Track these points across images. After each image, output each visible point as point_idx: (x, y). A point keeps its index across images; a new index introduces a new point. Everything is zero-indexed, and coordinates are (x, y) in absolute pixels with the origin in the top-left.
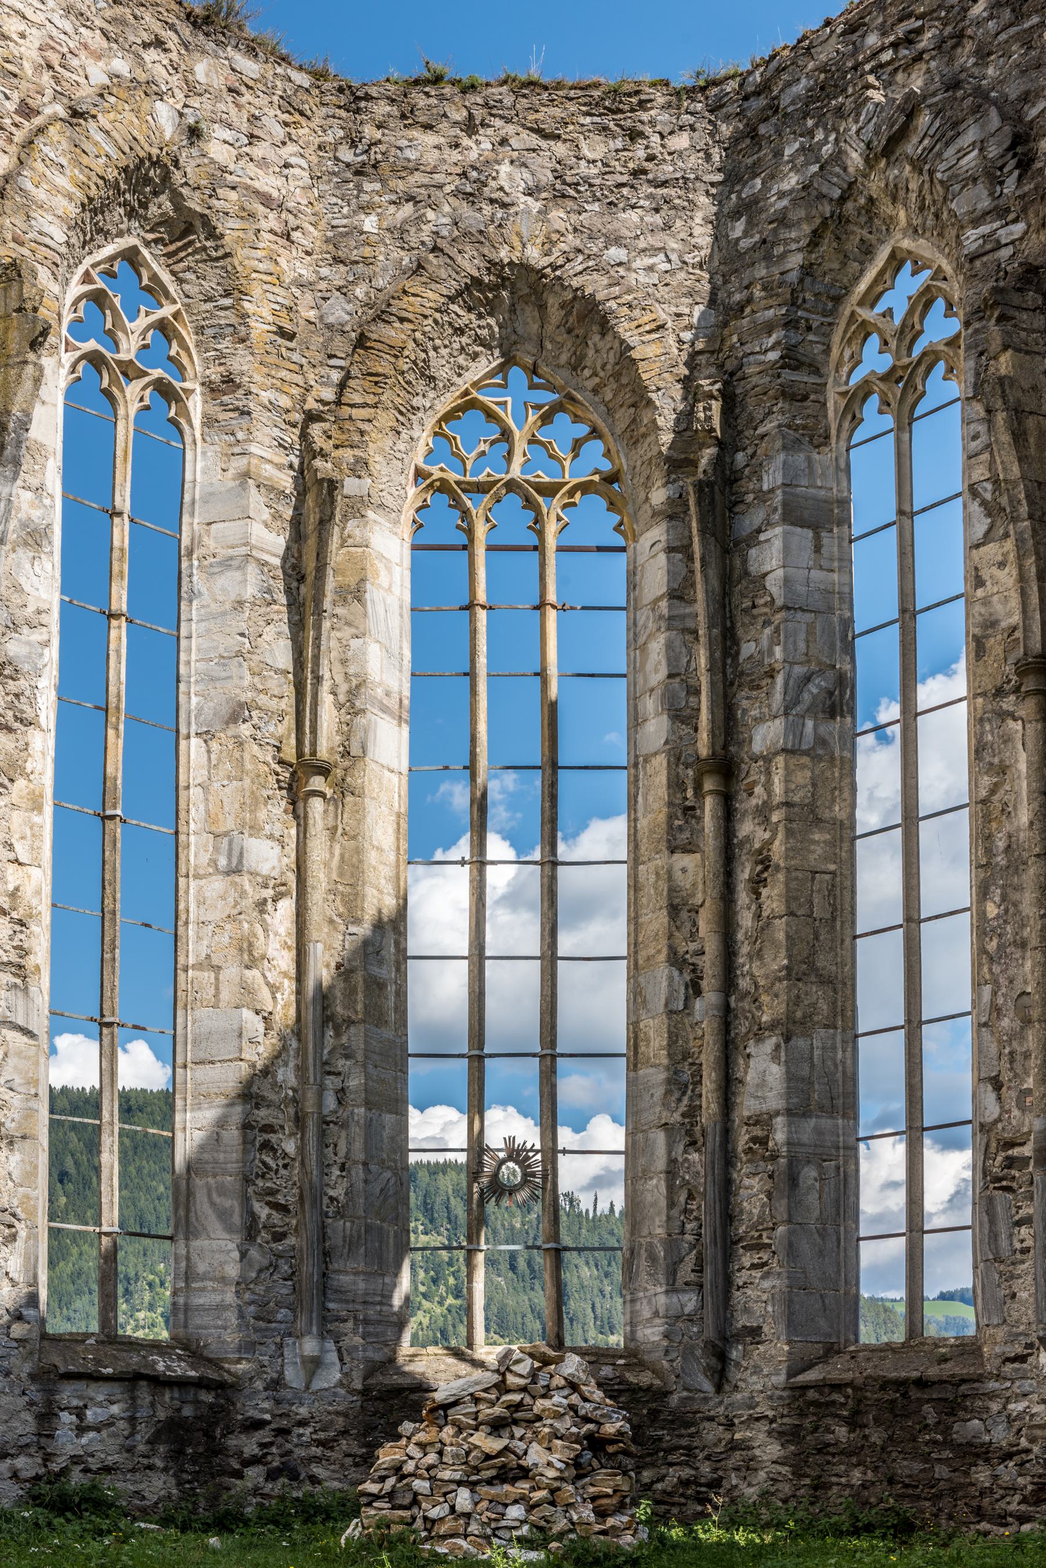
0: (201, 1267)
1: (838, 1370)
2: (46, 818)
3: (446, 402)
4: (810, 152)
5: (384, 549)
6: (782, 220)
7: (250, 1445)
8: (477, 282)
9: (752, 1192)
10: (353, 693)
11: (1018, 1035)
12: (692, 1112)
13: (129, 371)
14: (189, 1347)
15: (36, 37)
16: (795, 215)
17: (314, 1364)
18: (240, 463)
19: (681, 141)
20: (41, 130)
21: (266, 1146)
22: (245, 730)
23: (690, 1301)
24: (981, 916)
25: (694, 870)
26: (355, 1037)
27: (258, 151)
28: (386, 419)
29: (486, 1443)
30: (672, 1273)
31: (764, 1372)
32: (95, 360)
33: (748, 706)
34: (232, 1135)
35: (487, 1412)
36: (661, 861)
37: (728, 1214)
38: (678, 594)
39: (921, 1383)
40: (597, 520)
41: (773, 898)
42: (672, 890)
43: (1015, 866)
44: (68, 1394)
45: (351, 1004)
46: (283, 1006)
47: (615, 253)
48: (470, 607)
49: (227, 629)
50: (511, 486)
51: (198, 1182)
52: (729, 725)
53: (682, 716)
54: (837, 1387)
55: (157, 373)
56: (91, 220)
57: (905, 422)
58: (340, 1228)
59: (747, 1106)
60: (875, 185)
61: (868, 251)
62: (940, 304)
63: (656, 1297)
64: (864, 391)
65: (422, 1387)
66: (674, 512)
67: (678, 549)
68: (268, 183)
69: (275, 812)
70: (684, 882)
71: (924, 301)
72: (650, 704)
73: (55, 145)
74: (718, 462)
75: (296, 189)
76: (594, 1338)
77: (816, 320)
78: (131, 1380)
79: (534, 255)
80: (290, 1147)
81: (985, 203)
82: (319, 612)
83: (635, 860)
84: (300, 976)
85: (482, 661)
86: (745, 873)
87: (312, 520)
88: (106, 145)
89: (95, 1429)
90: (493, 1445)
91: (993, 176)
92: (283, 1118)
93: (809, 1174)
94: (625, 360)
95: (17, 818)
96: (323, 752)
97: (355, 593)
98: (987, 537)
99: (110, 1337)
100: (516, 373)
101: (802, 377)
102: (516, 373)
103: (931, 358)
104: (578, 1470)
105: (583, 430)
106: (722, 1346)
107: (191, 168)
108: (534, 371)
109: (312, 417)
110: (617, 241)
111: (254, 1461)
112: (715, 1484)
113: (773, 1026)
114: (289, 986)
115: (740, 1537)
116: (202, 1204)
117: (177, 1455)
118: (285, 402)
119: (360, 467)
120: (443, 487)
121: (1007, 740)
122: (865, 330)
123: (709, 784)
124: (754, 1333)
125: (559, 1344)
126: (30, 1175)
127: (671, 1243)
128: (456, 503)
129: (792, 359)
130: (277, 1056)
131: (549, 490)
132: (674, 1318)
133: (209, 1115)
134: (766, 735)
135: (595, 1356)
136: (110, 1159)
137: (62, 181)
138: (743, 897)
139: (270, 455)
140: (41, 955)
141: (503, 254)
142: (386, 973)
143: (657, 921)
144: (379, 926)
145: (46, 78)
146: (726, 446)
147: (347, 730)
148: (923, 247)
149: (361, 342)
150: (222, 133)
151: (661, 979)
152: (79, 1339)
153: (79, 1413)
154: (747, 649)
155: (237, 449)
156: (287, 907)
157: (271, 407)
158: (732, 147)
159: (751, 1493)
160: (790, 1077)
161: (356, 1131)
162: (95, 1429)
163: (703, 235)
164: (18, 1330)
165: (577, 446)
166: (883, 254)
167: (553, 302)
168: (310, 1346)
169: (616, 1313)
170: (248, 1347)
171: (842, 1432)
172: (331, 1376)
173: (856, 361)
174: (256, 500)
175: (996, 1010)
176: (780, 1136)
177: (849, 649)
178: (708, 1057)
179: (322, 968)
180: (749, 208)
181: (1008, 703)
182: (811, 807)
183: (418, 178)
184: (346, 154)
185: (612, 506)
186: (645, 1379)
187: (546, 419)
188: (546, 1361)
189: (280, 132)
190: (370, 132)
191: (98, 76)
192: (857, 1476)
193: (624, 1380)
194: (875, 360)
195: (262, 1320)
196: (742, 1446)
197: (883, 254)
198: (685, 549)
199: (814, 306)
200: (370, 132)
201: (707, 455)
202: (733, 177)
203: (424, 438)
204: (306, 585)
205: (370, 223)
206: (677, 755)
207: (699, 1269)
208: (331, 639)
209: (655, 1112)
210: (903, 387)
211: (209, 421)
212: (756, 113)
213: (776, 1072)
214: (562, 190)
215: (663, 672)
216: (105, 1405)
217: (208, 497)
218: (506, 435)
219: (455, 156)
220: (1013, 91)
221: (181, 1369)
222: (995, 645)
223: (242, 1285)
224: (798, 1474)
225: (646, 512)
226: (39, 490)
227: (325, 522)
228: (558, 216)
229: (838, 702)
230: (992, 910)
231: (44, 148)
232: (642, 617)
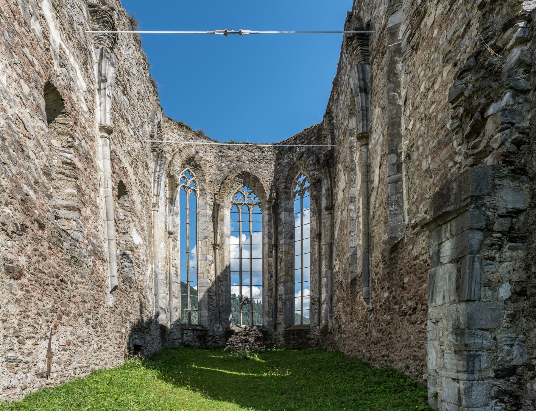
0: (202, 315)
1: (291, 328)
2: (179, 254)
3: (235, 191)
4: (289, 157)
5: (226, 213)
6: (285, 167)
7: (210, 339)
8: (240, 174)
9: (280, 304)
10: (222, 234)
11: (315, 284)
12: (271, 294)
13: (189, 188)
14: (202, 326)
15: (174, 139)
16: (287, 166)
17: (218, 328)
18: (205, 201)
19: (270, 153)
20: (175, 154)
21: (211, 298)
22: (207, 240)
23: (271, 319)
24: (311, 268)
25: (272, 260)
26: (223, 283)
27: (207, 154)
28: (226, 194)
29: (243, 337)
30: (269, 315)
31: (281, 329)
32: (184, 186)
33: (279, 237)
34: (206, 296)
35: (243, 334)
36: (267, 259)
38: (269, 221)
39: (302, 330)
40: (257, 209)
41: (283, 264)
42: (269, 263)
43: (315, 262)
44: (185, 332)
45: (223, 278)
46: (213, 279)
47: (260, 170)
48: (239, 222)
49: (204, 225)
50: (245, 204)
51: (202, 303)
52: (277, 240)
53: (270, 238)
54: (291, 331)
55: (193, 188)
56: (183, 166)
57: (302, 198)
58: (222, 309)
59: (279, 293)
60: (298, 163)
61: (297, 172)
62: (307, 181)
63: (266, 319)
64: (296, 192)
65: (233, 331)
66: (269, 209)
67: (269, 214)
69: (212, 251)
70: (270, 262)
71: (304, 181)
72: (265, 236)
73: (177, 156)
74: (275, 202)
75: (212, 159)
76: (257, 324)
77: (289, 182)
78: (193, 330)
79: (248, 170)
80: (214, 298)
81: (313, 169)
82: (217, 223)
83: (263, 258)
84: (215, 275)
85: (241, 229)
86: (279, 261)
87: (216, 210)
88: (185, 156)
89: (189, 336)
90: (245, 338)
91: (314, 165)
92: (213, 294)
93: (288, 302)
94: (262, 186)
95: (176, 253)
96: (218, 243)
97: (222, 220)
98: (312, 216)
99: (190, 324)
100: (246, 187)
101: (288, 190)
102: (246, 187)
103: (305, 189)
104: (256, 341)
105: (255, 196)
106: (276, 326)
107: (197, 158)
108: (248, 187)
109: (215, 194)
110: (260, 168)
111: (210, 341)
112: (275, 344)
113: (283, 282)
114: (214, 276)
115: (278, 350)
116: (202, 306)
117: (200, 340)
118: (211, 192)
119: (223, 201)
120: (235, 204)
121: (315, 244)
122: (296, 184)
123: (274, 248)
124: (280, 323)
125: (253, 325)
126: (179, 303)
127: (268, 311)
128: (237, 206)
129: (286, 187)
130: (212, 286)
131: (251, 205)
133: (203, 294)
134: (282, 241)
135: (258, 327)
136: (189, 300)
137: (179, 161)
138: (279, 264)
139: (209, 199)
140: (179, 273)
141: (244, 170)
142: (228, 274)
143: (266, 267)
144: (226, 267)
145: (176, 145)
146: (276, 199)
147: (222, 240)
148: (304, 173)
149: (223, 183)
150: (201, 152)
151: (267, 275)
152: (185, 324)
153: (187, 334)
154: (279, 229)
155: (205, 199)
156: (213, 265)
157: (209, 193)
158: (277, 154)
159: (279, 345)
160: (285, 289)
161: (224, 296)
162: (189, 336)
163: (273, 168)
164: (178, 323)
165: (255, 198)
166: (299, 173)
167: (251, 177)
168: (218, 325)
169: (260, 320)
170: (209, 325)
171: (292, 336)
172: (221, 329)
173: (295, 188)
174: (208, 207)
175: (313, 281)
176: (284, 297)
177: (294, 230)
178: (274, 286)
179: (218, 273)
180: (280, 164)
181: (315, 239)
182: (288, 252)
183: (231, 158)
184: (220, 154)
185: (260, 207)
186: (265, 330)
187: (250, 194)
188: (251, 327)
189: (210, 151)
190: (223, 151)
191: (183, 145)
192: (294, 342)
193: (261, 329)
194: (298, 188)
195: (211, 321)
196: (278, 338)
197: (299, 173)
198: (270, 214)
199: (290, 180)
200: (223, 151)
201: (274, 201)
202: (278, 159)
203: (232, 197)
204: (215, 219)
205: (223, 165)
206: (269, 244)
207: (272, 315)
208: (219, 226)
209: (266, 294)
210: (302, 193)
211: (200, 195)
212: (281, 151)
213: (283, 288)
214: (252, 160)
215: (267, 232)
216: (190, 333)
217: (201, 206)
218: (244, 196)
219: (236, 155)
220: (317, 152)
221: (200, 328)
222: (313, 231)
223: (208, 317)
224: (286, 342)
225: (265, 209)
226: (177, 207)
227: (218, 210)
228: (251, 164)
230: (312, 268)
232: (264, 223)
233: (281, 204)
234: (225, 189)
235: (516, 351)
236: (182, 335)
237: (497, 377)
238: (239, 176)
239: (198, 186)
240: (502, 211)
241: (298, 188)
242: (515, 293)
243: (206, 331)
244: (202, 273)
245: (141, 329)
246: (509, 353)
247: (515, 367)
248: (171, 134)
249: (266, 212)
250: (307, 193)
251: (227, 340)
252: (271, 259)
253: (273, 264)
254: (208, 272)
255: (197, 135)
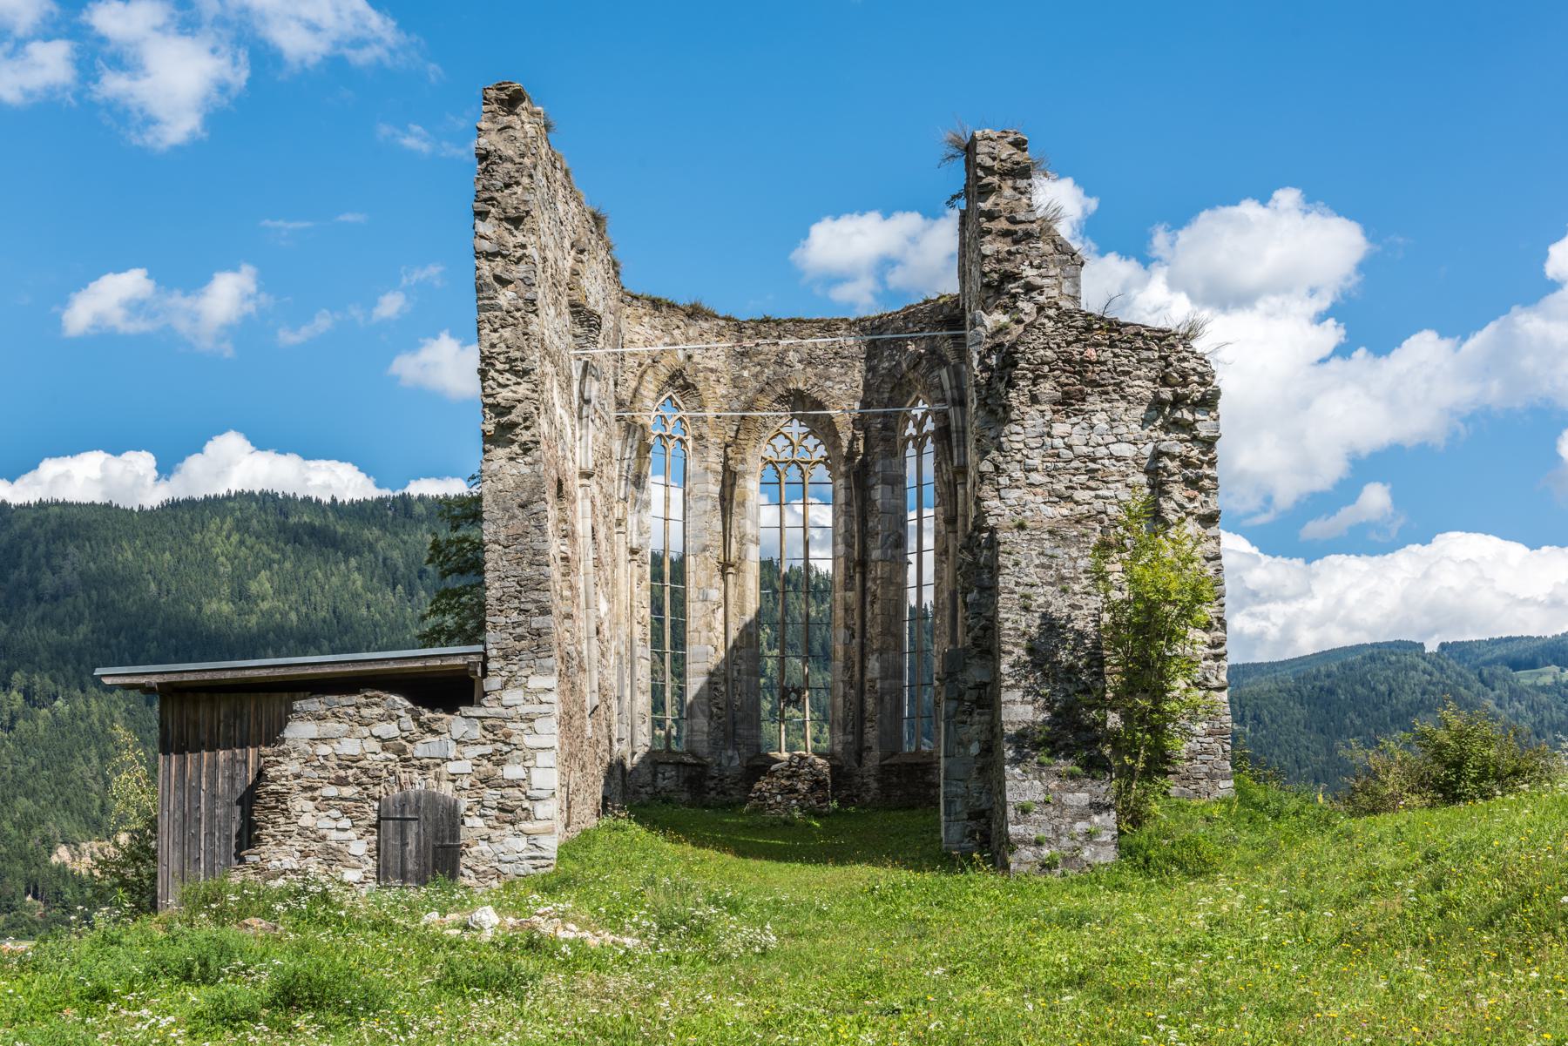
1: (894, 760)
7: (712, 784)
9: (870, 703)
10: (742, 538)
12: (851, 677)
13: (671, 437)
14: (694, 755)
18: (704, 465)
23: (850, 738)
28: (752, 443)
31: (873, 760)
33: (871, 543)
37: (862, 710)
38: (848, 504)
41: (877, 607)
44: (660, 769)
47: (829, 383)
52: (864, 550)
53: (849, 545)
57: (920, 455)
59: (869, 675)
60: (911, 376)
61: (909, 394)
63: (840, 736)
64: (908, 439)
66: (846, 476)
68: (712, 364)
69: (717, 580)
71: (925, 415)
72: (839, 540)
73: (649, 377)
79: (801, 386)
86: (869, 599)
88: (663, 371)
93: (887, 698)
97: (742, 504)
103: (926, 436)
104: (812, 790)
106: (860, 752)
110: (828, 379)
119: (743, 461)
127: (844, 719)
132: (845, 744)
134: (876, 554)
139: (714, 459)
147: (740, 550)
155: (703, 459)
156: (721, 610)
168: (730, 753)
170: (711, 753)
174: (710, 477)
178: (857, 659)
195: (714, 744)
205: (746, 374)
206: (847, 558)
211: (694, 449)
213: (877, 665)
216: (671, 772)
221: (690, 760)
223: (709, 734)
227: (733, 485)
228: (809, 369)
229: (900, 543)
231: (647, 378)
233: (874, 464)
234: (748, 431)
235: (984, 798)
236: (655, 775)
237: (970, 818)
238: (781, 399)
239: (690, 430)
240: (971, 684)
241: (911, 430)
242: (982, 750)
243: (705, 766)
244: (696, 630)
245: (615, 771)
246: (979, 799)
247: (984, 811)
248: (638, 328)
249: (841, 481)
250: (929, 446)
251: (750, 788)
252: (850, 594)
253: (856, 606)
254: (710, 628)
255: (689, 316)
